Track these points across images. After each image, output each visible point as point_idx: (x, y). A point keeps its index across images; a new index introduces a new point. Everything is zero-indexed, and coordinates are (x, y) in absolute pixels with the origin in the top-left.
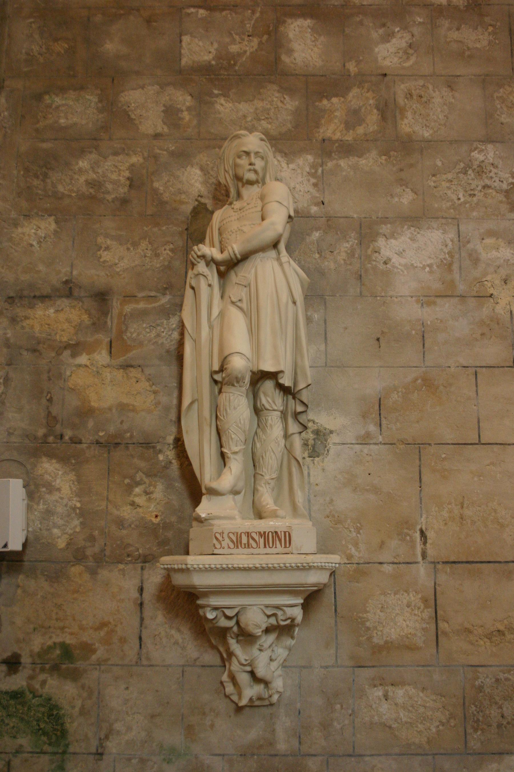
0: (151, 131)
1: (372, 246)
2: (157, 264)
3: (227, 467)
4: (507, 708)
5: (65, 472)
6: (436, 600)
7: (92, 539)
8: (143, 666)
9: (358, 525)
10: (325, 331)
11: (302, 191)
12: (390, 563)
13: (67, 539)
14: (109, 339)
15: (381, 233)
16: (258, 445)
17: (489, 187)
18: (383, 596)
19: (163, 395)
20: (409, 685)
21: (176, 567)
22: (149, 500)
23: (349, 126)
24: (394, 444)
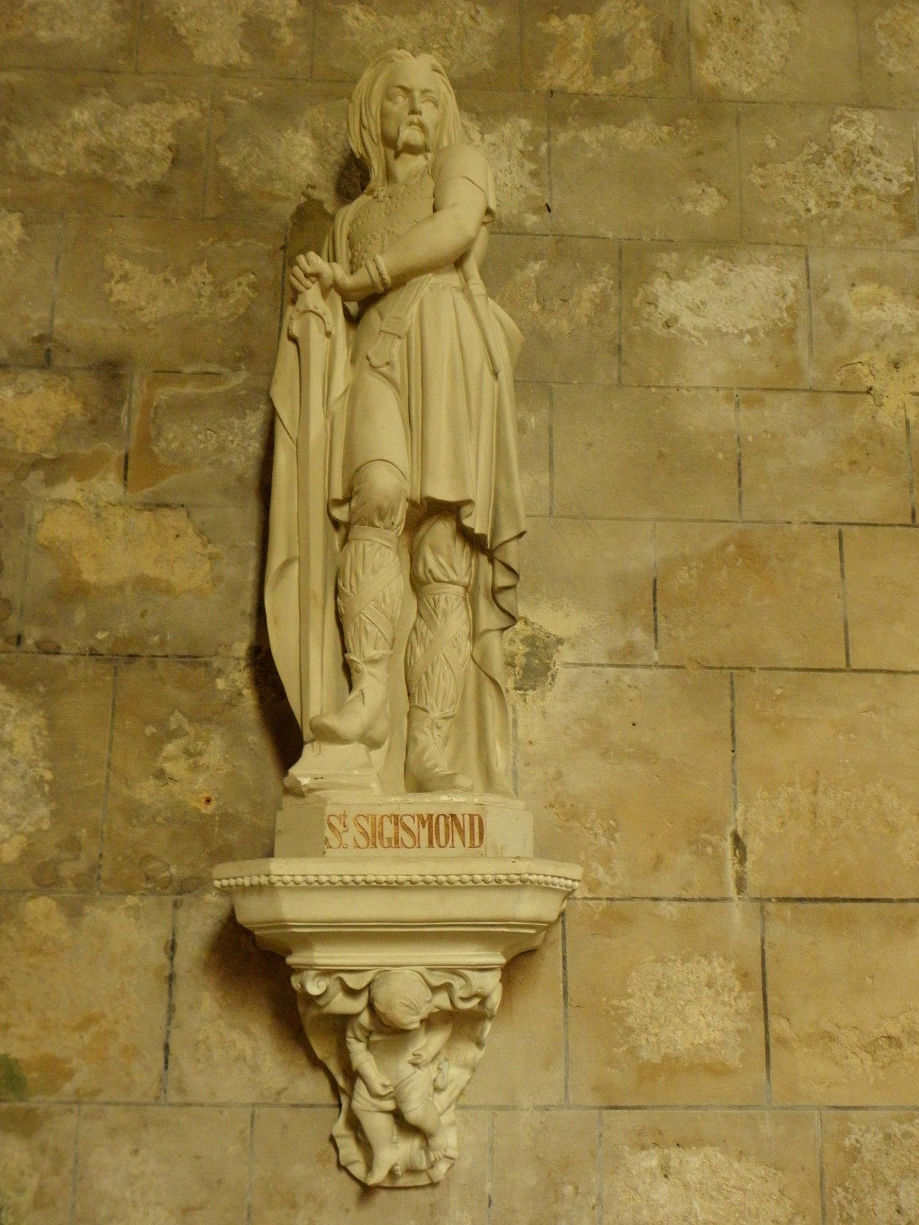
0: (217, 61)
1: (641, 293)
2: (223, 309)
3: (355, 693)
4: (907, 1193)
5: (24, 710)
6: (764, 974)
7: (72, 845)
8: (170, 1105)
9: (611, 822)
10: (551, 448)
11: (510, 185)
12: (676, 899)
13: (21, 843)
14: (123, 452)
15: (659, 269)
16: (419, 651)
17: (865, 190)
18: (659, 964)
19: (228, 563)
20: (712, 1145)
21: (247, 882)
22: (195, 768)
23: (599, 68)
24: (683, 667)
